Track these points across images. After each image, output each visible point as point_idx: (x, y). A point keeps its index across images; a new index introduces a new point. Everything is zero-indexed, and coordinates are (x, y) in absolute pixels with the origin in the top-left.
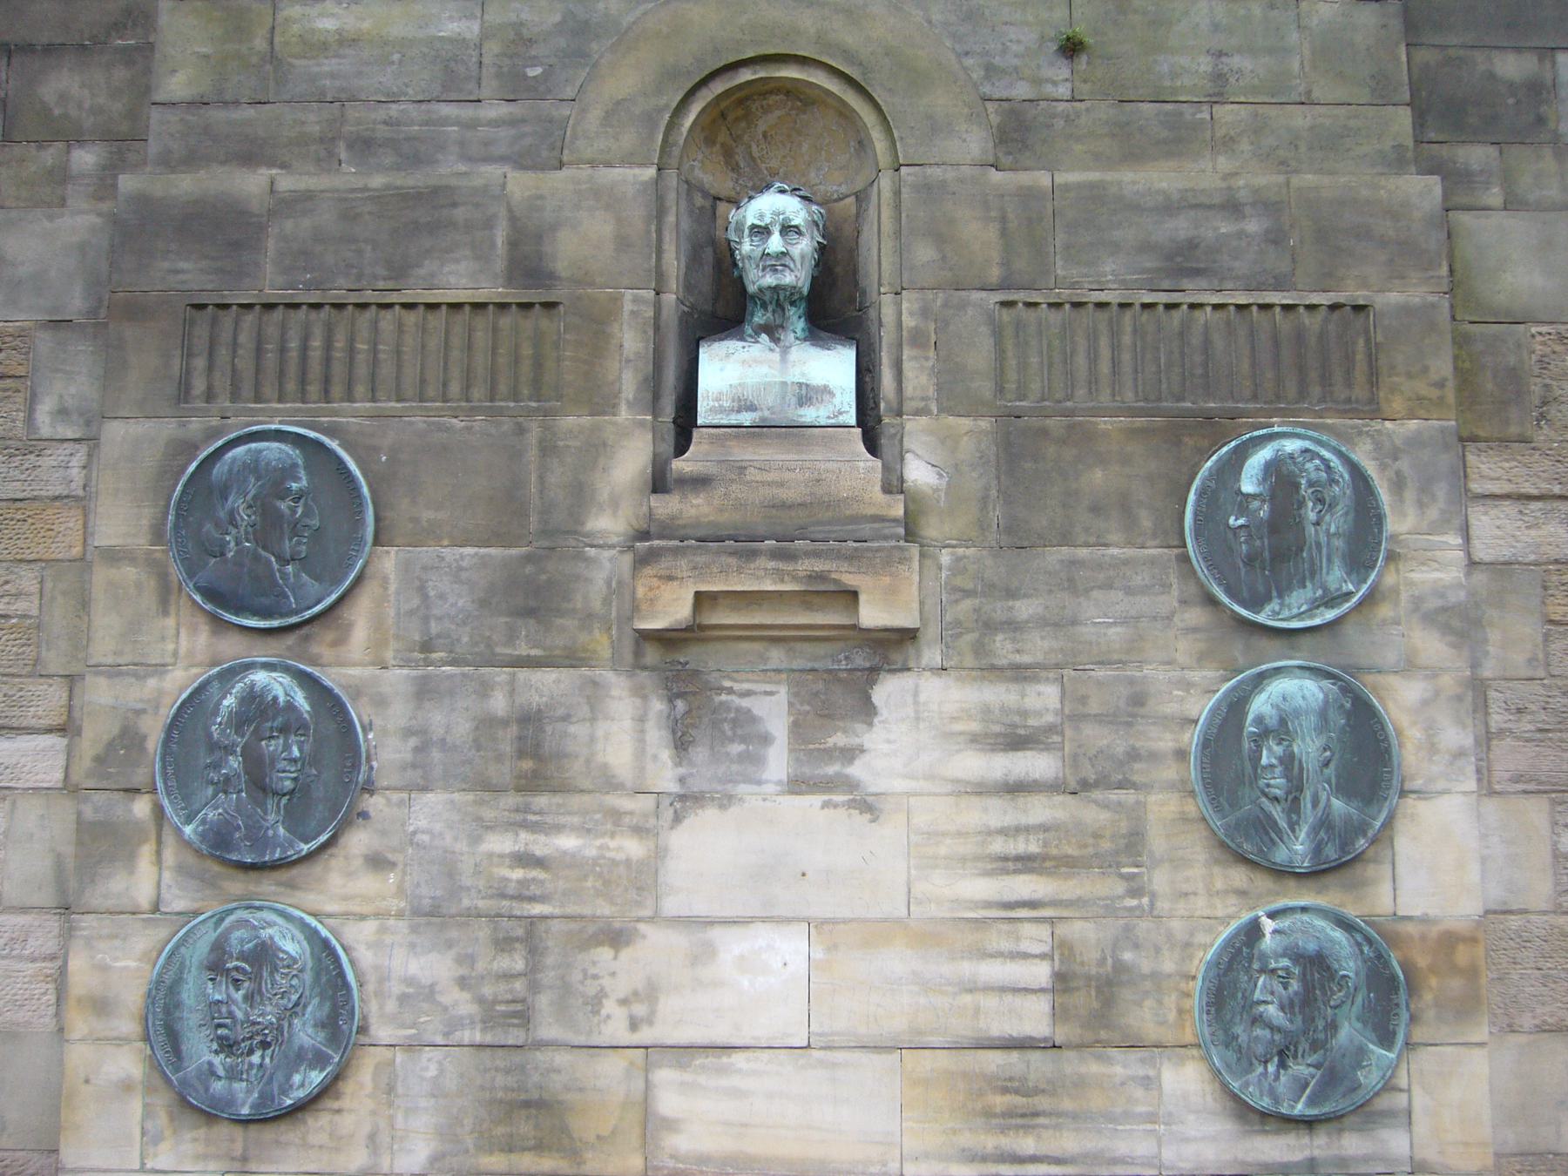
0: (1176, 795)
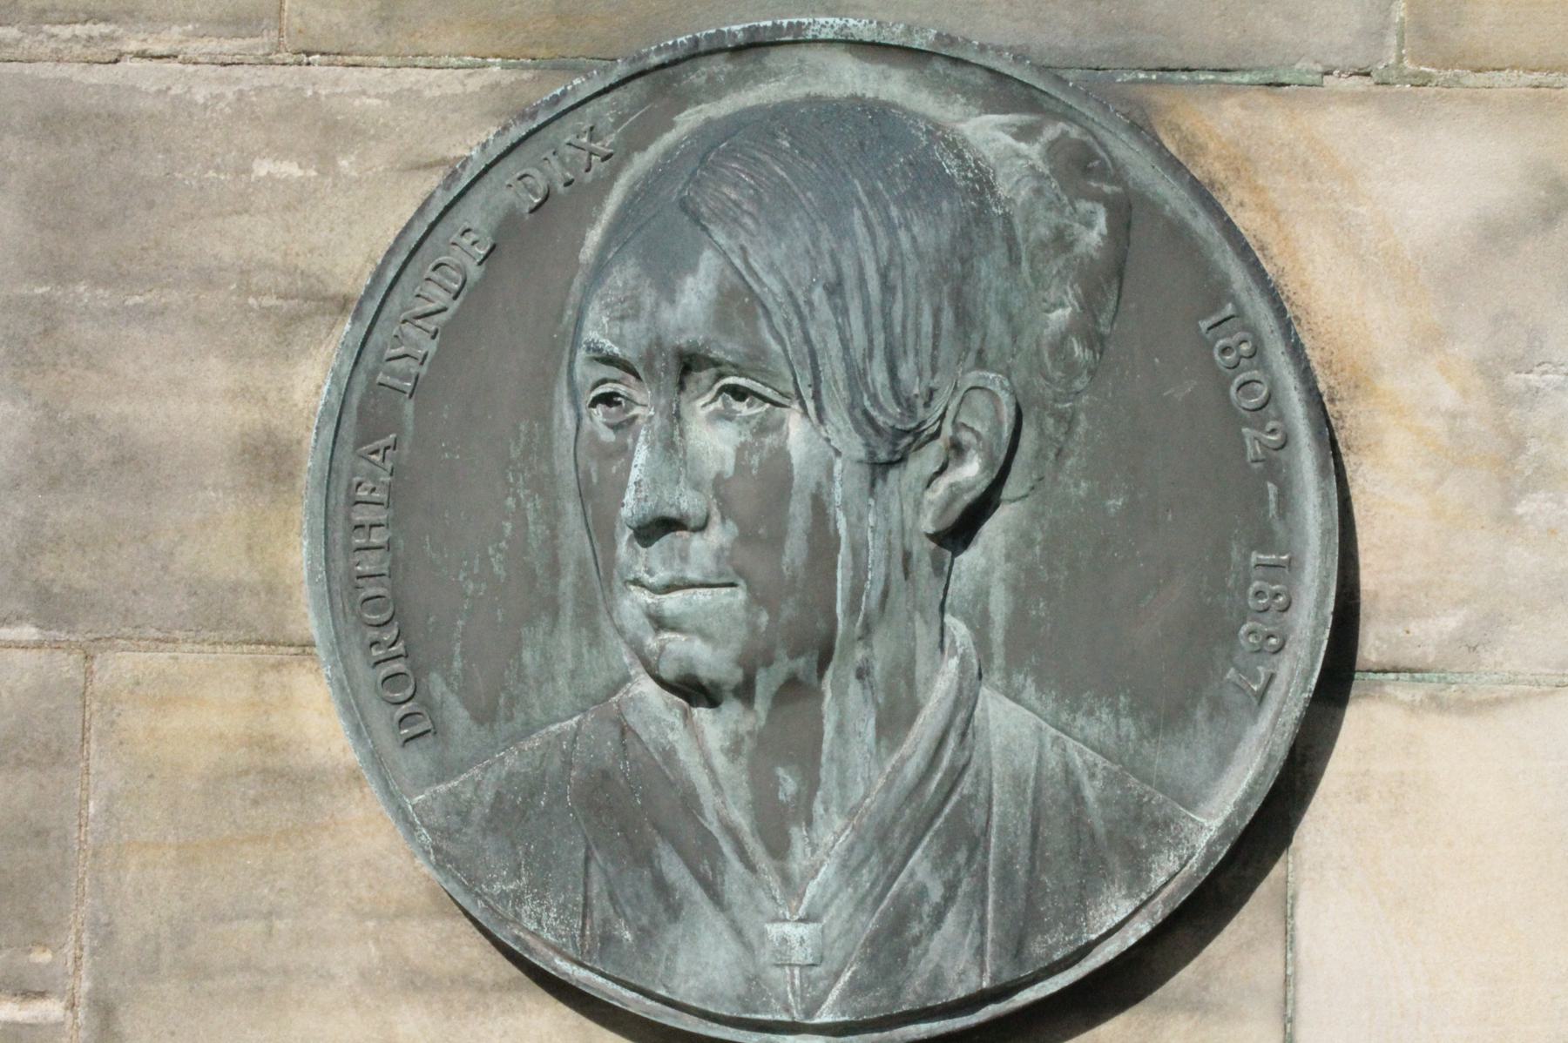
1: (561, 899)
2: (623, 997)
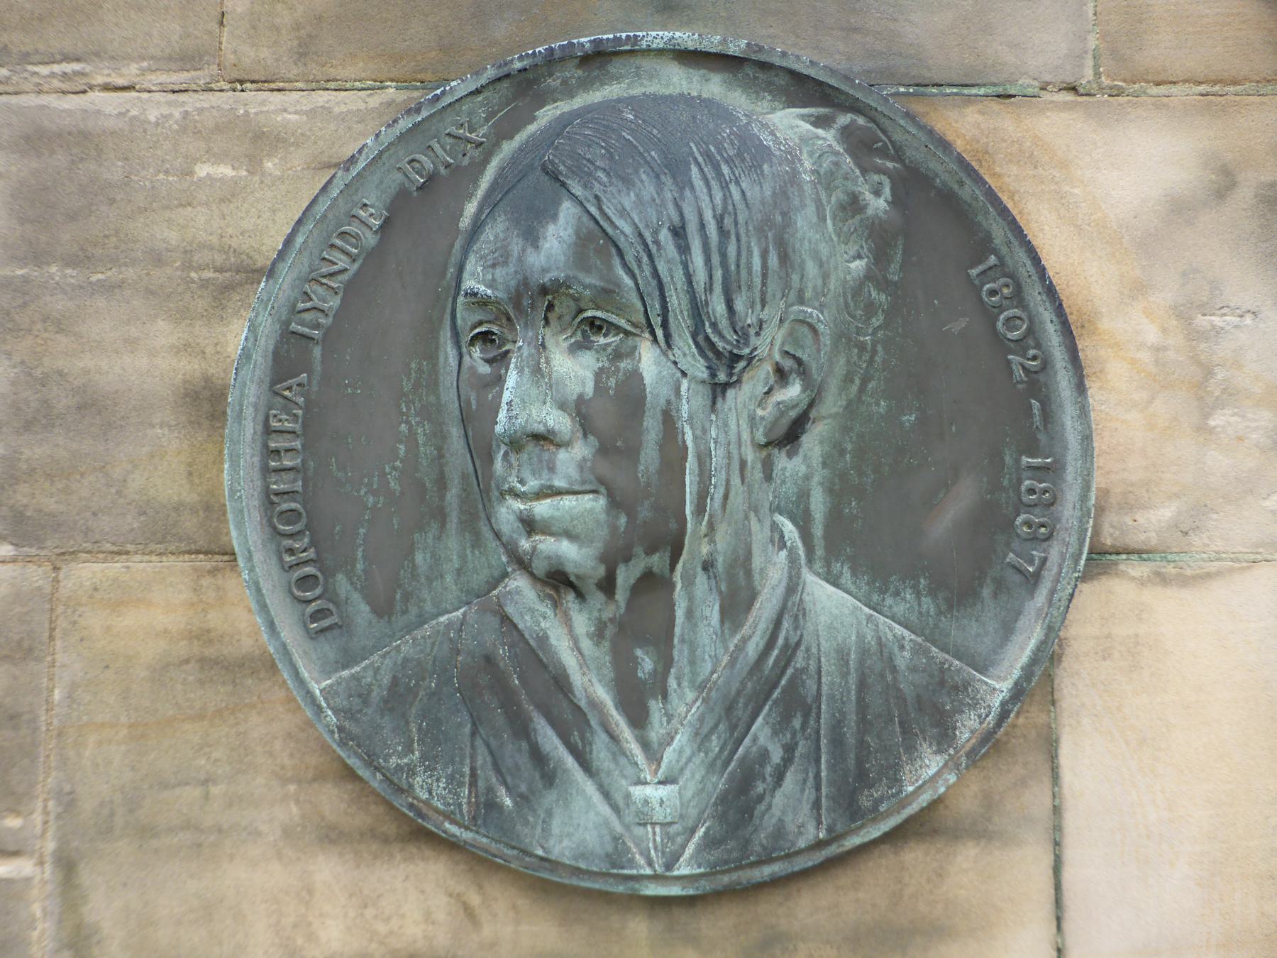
0: (180, 565)
1: (449, 771)
2: (504, 854)
